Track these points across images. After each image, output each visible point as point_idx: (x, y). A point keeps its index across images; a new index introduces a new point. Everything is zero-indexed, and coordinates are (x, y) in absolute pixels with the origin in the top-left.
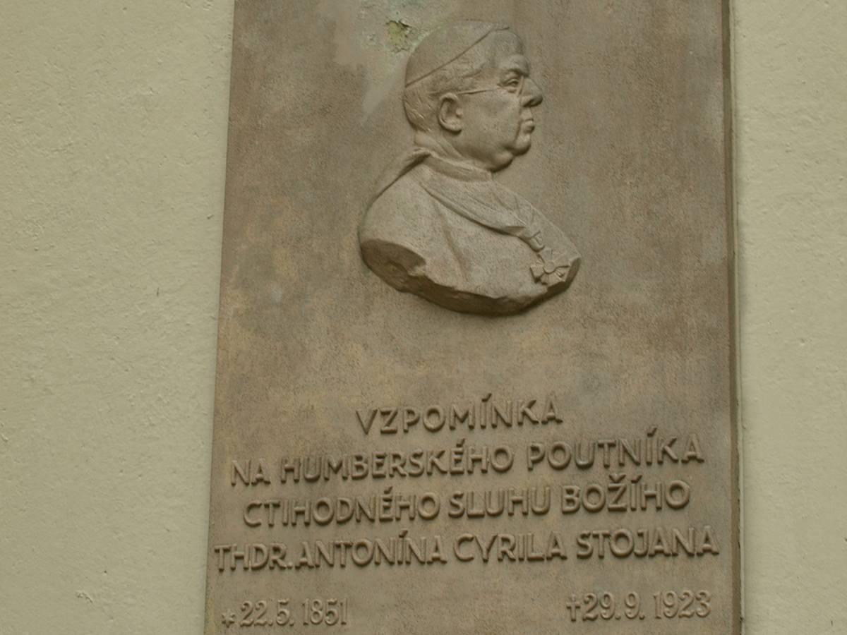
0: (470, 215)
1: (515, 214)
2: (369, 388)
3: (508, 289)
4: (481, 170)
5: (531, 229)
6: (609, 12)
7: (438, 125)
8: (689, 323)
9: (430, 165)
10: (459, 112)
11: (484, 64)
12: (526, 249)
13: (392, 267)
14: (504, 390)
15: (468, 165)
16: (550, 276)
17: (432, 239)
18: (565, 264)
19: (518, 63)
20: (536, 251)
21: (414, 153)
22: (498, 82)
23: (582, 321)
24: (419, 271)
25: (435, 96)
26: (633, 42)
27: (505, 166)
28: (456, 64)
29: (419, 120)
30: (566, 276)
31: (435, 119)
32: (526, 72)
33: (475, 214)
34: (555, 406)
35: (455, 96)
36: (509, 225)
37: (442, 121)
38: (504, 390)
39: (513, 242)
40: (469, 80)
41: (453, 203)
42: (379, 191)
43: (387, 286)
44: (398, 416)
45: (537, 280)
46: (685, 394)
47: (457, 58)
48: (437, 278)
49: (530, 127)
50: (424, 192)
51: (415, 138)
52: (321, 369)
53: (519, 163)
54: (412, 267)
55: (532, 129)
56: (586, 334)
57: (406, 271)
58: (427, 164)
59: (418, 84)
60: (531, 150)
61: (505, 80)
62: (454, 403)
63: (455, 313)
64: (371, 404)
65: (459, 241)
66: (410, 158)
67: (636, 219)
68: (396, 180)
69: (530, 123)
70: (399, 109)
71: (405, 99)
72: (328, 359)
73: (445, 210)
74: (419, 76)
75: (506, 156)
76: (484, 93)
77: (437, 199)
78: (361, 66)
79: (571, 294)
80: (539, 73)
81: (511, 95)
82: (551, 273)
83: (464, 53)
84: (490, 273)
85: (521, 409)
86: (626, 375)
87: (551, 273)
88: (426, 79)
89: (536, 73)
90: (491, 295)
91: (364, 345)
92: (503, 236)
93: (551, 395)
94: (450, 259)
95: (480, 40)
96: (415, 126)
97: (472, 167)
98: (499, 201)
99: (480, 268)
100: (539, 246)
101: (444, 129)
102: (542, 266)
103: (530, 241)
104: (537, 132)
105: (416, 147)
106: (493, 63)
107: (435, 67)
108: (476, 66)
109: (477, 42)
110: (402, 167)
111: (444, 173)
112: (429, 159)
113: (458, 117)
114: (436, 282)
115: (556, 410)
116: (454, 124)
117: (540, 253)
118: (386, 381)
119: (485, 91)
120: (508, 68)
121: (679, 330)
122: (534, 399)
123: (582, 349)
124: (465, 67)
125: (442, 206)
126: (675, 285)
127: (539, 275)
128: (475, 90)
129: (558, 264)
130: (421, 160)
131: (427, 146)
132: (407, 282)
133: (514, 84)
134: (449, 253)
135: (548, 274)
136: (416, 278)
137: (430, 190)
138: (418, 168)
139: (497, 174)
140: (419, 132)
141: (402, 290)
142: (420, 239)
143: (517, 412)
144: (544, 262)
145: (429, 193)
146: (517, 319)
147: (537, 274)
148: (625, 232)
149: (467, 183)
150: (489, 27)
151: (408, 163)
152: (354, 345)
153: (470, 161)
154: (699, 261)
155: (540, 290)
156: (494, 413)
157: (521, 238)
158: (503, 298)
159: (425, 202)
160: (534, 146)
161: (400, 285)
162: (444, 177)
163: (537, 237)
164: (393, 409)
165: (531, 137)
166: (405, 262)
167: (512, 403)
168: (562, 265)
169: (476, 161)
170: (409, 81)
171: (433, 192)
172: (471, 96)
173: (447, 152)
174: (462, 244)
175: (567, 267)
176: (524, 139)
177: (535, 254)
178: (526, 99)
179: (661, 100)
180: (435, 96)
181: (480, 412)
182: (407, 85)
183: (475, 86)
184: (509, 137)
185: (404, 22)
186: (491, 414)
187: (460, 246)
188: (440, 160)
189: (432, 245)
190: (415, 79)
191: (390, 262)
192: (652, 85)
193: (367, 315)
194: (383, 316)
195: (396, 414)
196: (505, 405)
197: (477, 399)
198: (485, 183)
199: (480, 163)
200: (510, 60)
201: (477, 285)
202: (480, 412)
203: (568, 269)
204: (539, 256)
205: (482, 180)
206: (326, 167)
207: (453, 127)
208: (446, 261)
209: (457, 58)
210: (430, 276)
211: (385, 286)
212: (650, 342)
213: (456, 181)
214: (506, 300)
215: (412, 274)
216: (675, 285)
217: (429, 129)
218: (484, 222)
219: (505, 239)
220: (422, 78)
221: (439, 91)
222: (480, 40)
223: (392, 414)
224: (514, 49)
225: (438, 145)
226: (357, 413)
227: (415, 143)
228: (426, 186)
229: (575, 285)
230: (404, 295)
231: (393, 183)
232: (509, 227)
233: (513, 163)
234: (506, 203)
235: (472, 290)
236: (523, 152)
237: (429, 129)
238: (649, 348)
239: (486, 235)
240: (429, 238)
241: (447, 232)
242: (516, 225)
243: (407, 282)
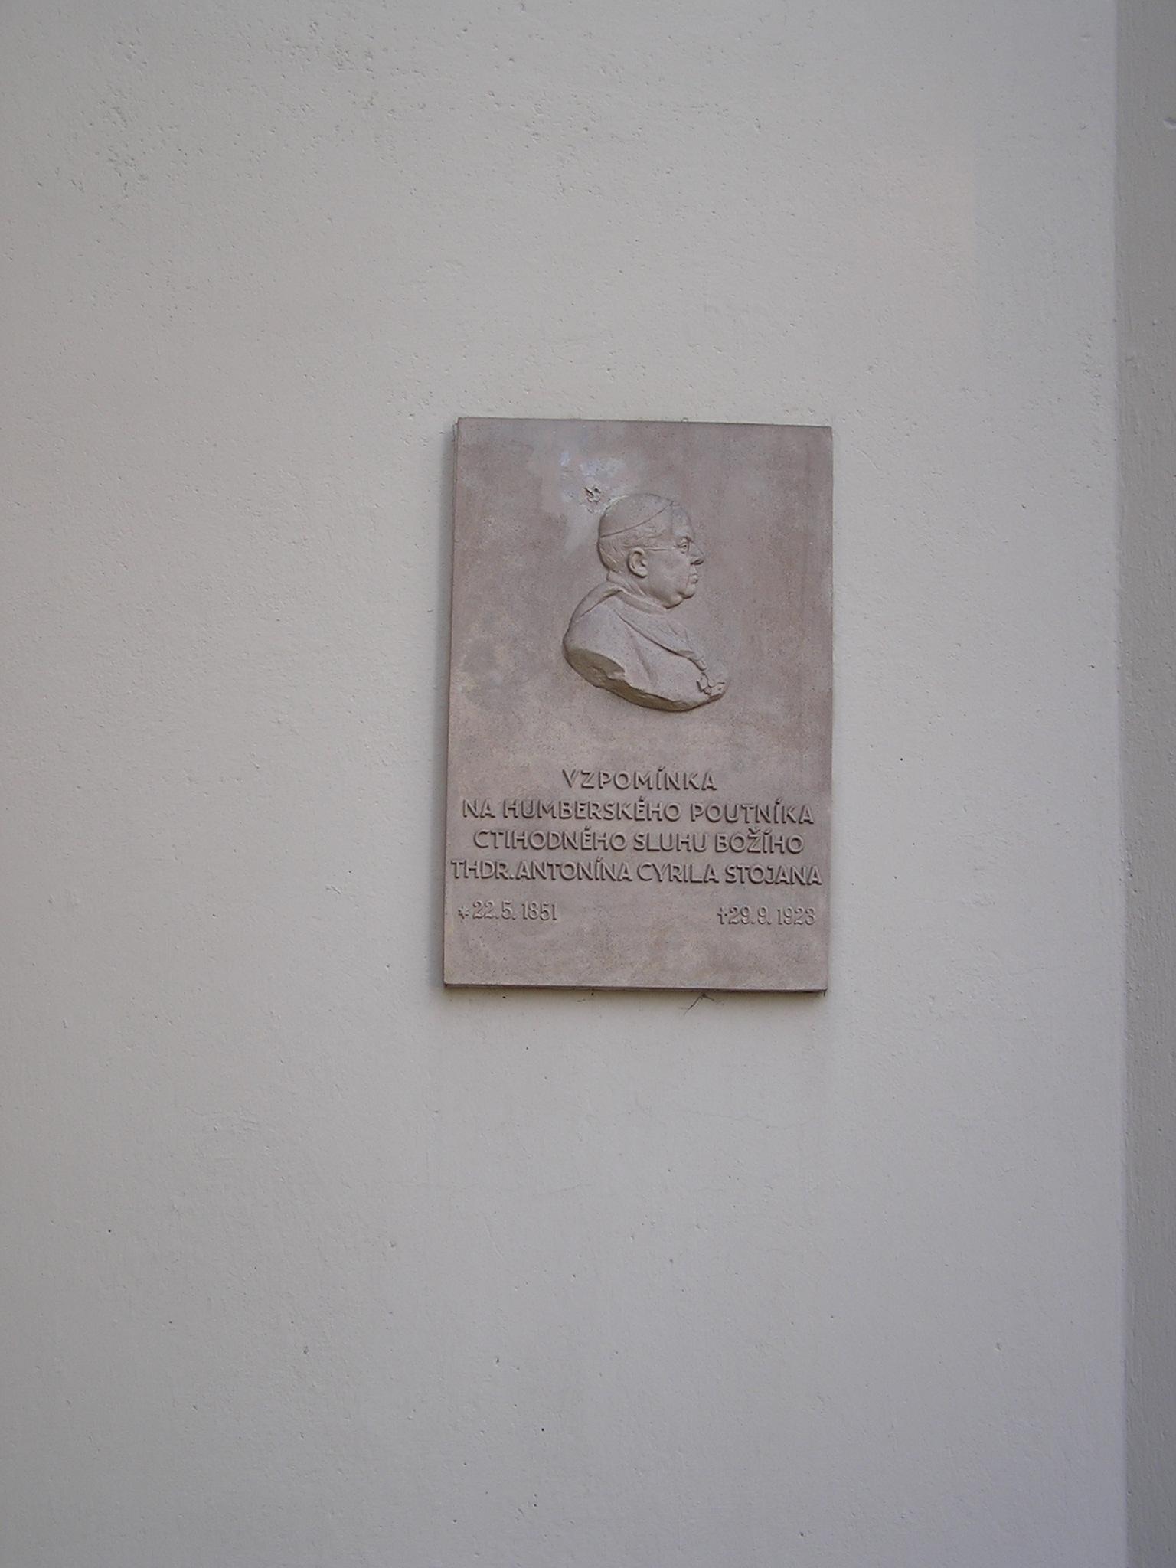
9: (621, 598)
12: (694, 668)
15: (649, 601)
24: (617, 675)
30: (722, 690)
40: (654, 540)
43: (586, 682)
47: (645, 522)
50: (618, 617)
59: (613, 537)
69: (695, 577)
77: (629, 624)
107: (628, 527)
108: (659, 532)
137: (622, 616)
153: (651, 599)
155: (702, 697)
166: (606, 668)
170: (603, 534)
172: (654, 552)
176: (690, 588)
177: (700, 672)
195: (593, 775)
199: (659, 601)
204: (704, 674)
209: (645, 522)
218: (664, 646)
228: (620, 614)
241: (638, 650)
243: (604, 681)
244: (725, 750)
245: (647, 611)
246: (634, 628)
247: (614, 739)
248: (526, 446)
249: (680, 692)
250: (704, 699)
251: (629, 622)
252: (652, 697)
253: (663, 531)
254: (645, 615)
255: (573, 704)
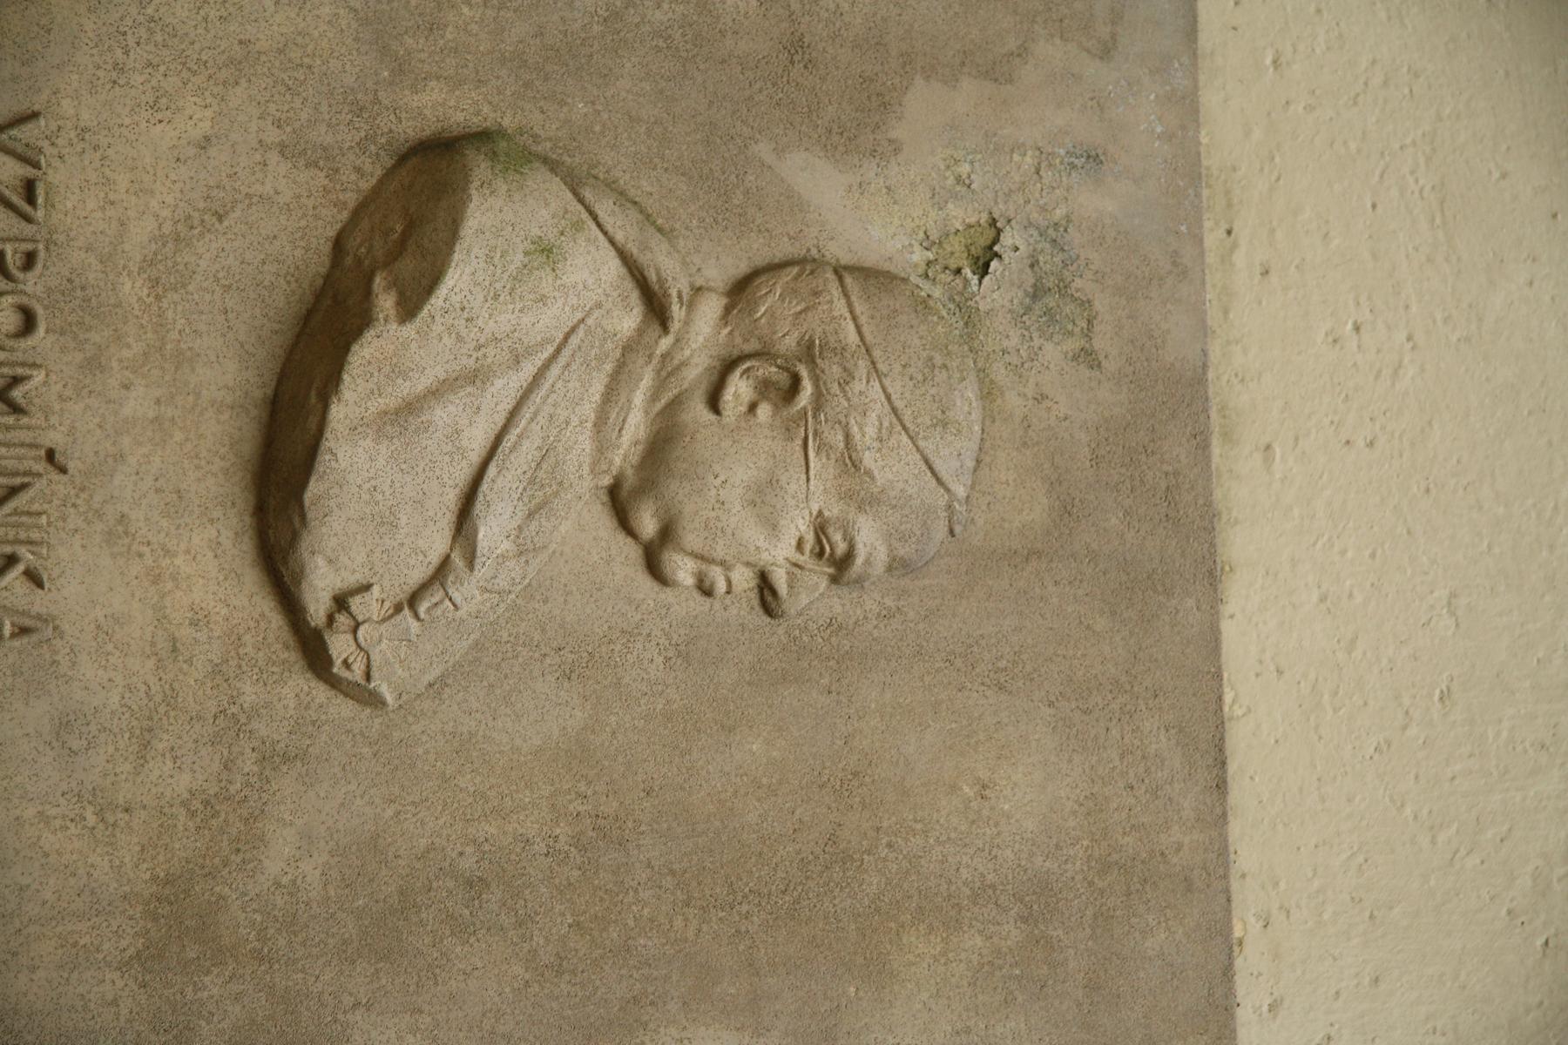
0: (511, 438)
1: (506, 546)
2: (96, 148)
3: (324, 530)
4: (618, 461)
5: (467, 591)
6: (966, 789)
7: (736, 353)
8: (207, 980)
9: (640, 332)
10: (764, 411)
11: (873, 478)
12: (417, 575)
13: (399, 228)
14: (74, 505)
15: (635, 425)
16: (350, 637)
17: (459, 338)
18: (375, 674)
19: (868, 562)
20: (413, 600)
21: (674, 293)
22: (826, 513)
23: (234, 709)
24: (386, 303)
25: (809, 352)
26: (889, 845)
27: (624, 522)
28: (879, 408)
29: (753, 306)
30: (345, 674)
31: (753, 346)
32: (845, 579)
33: (513, 449)
34: (25, 640)
35: (802, 404)
36: (480, 536)
37: (745, 367)
38: (74, 505)
39: (438, 542)
40: (838, 439)
41: (543, 392)
42: (588, 194)
43: (352, 205)
44: (24, 223)
45: (341, 602)
46: (33, 969)
47: (894, 410)
48: (364, 353)
49: (712, 585)
50: (579, 315)
51: (710, 289)
52: (152, 20)
53: (631, 552)
54: (394, 284)
55: (706, 590)
56: (199, 718)
57: (386, 265)
58: (643, 321)
59: (840, 306)
60: (655, 586)
61: (830, 530)
62: (47, 375)
63: (274, 384)
64: (55, 151)
65: (451, 408)
66: (661, 281)
67: (469, 850)
68: (612, 242)
69: (721, 586)
70: (784, 249)
71: (807, 263)
72: (176, 40)
73: (529, 369)
74: (858, 309)
75: (648, 525)
76: (804, 477)
77: (558, 351)
78: (897, 151)
79: (300, 685)
80: (838, 609)
81: (794, 543)
82: (356, 639)
83: (904, 428)
84: (367, 486)
85: (23, 551)
86: (91, 819)
87: (356, 639)
88: (851, 327)
89: (838, 604)
90: (314, 488)
91: (207, 139)
92: (454, 519)
93: (55, 628)
94: (408, 383)
95: (931, 468)
96: (741, 290)
97: (626, 438)
98: (539, 507)
99: (381, 461)
100: (422, 609)
101: (728, 366)
102: (375, 618)
103: (437, 586)
104: (699, 603)
105: (686, 291)
106: (867, 502)
107: (877, 353)
108: (868, 459)
109: (927, 462)
110: (644, 259)
111: (620, 367)
112: (655, 329)
113: (752, 407)
114: (355, 348)
115: (17, 643)
116: (736, 395)
117: (406, 611)
118: (112, 196)
119: (808, 480)
120: (858, 539)
121: (193, 955)
122: (47, 585)
123: (162, 709)
124: (871, 431)
125: (539, 363)
126: (304, 944)
127: (353, 608)
128: (812, 454)
129: (376, 659)
130: (656, 307)
131: (687, 323)
132: (359, 262)
133: (817, 550)
134: (422, 383)
135: (355, 631)
136: (368, 293)
137: (581, 332)
138: (635, 296)
139: (605, 498)
140: (724, 301)
141: (338, 245)
142: (463, 309)
143: (17, 542)
144: (384, 620)
145: (573, 330)
146: (248, 545)
147: (355, 603)
148: (441, 822)
149: (589, 425)
150: (961, 491)
151: (652, 276)
152: (209, 113)
153: (642, 434)
154: (356, 1005)
155: (317, 606)
156: (18, 481)
157: (444, 565)
158: (303, 516)
159: (549, 320)
160: (668, 595)
161: (353, 243)
162: (609, 367)
163: (447, 602)
164: (40, 214)
165: (687, 588)
166: (407, 266)
167: (39, 527)
168: (375, 665)
169: (640, 447)
170: (848, 280)
171: (574, 341)
172: (799, 442)
173: (670, 374)
174: (441, 415)
175: (368, 677)
176: (683, 569)
177: (403, 596)
178: (780, 579)
179: (747, 916)
180: (809, 352)
181: (22, 445)
182: (840, 271)
183: (824, 454)
184: (691, 538)
185: (994, 264)
186: (15, 474)
187: (438, 412)
188: (650, 356)
189: (446, 340)
190: (853, 298)
191: (411, 226)
192: (784, 892)
193: (282, 149)
194: (277, 193)
195: (28, 219)
196: (36, 507)
197: (54, 438)
198: (586, 469)
199: (635, 459)
200: (877, 544)
201: (340, 456)
202: (22, 445)
203: (360, 680)
204: (398, 609)
205: (594, 464)
206: (659, 50)
207: (728, 395)
208: (405, 375)
209: (894, 410)
210: (369, 335)
211: (352, 199)
212: (168, 882)
213: (597, 397)
214: (296, 520)
215: (379, 281)
216: (304, 944)
217: (729, 328)
218: (492, 470)
219: (446, 522)
220: (854, 319)
221: (819, 361)
222: (931, 468)
223: (27, 208)
224: (901, 552)
225: (687, 353)
226: (35, 115)
227: (700, 289)
228: (590, 321)
229: (321, 692)
230: (326, 248)
231: (605, 233)
232: (476, 532)
233: (629, 540)
234: (534, 525)
235: (329, 441)
236: (653, 565)
237: (729, 328)
238: (154, 878)
239: (461, 473)
240: (464, 332)
241: (476, 377)
242: (479, 554)
243: (359, 262)
244: (129, 687)
245: (601, 422)
246: (546, 366)
247: (158, 298)
248: (1113, 36)
249: (336, 523)
250: (312, 608)
251: (566, 352)
252: (312, 423)
253: (869, 473)
254: (588, 410)
255: (273, 157)
